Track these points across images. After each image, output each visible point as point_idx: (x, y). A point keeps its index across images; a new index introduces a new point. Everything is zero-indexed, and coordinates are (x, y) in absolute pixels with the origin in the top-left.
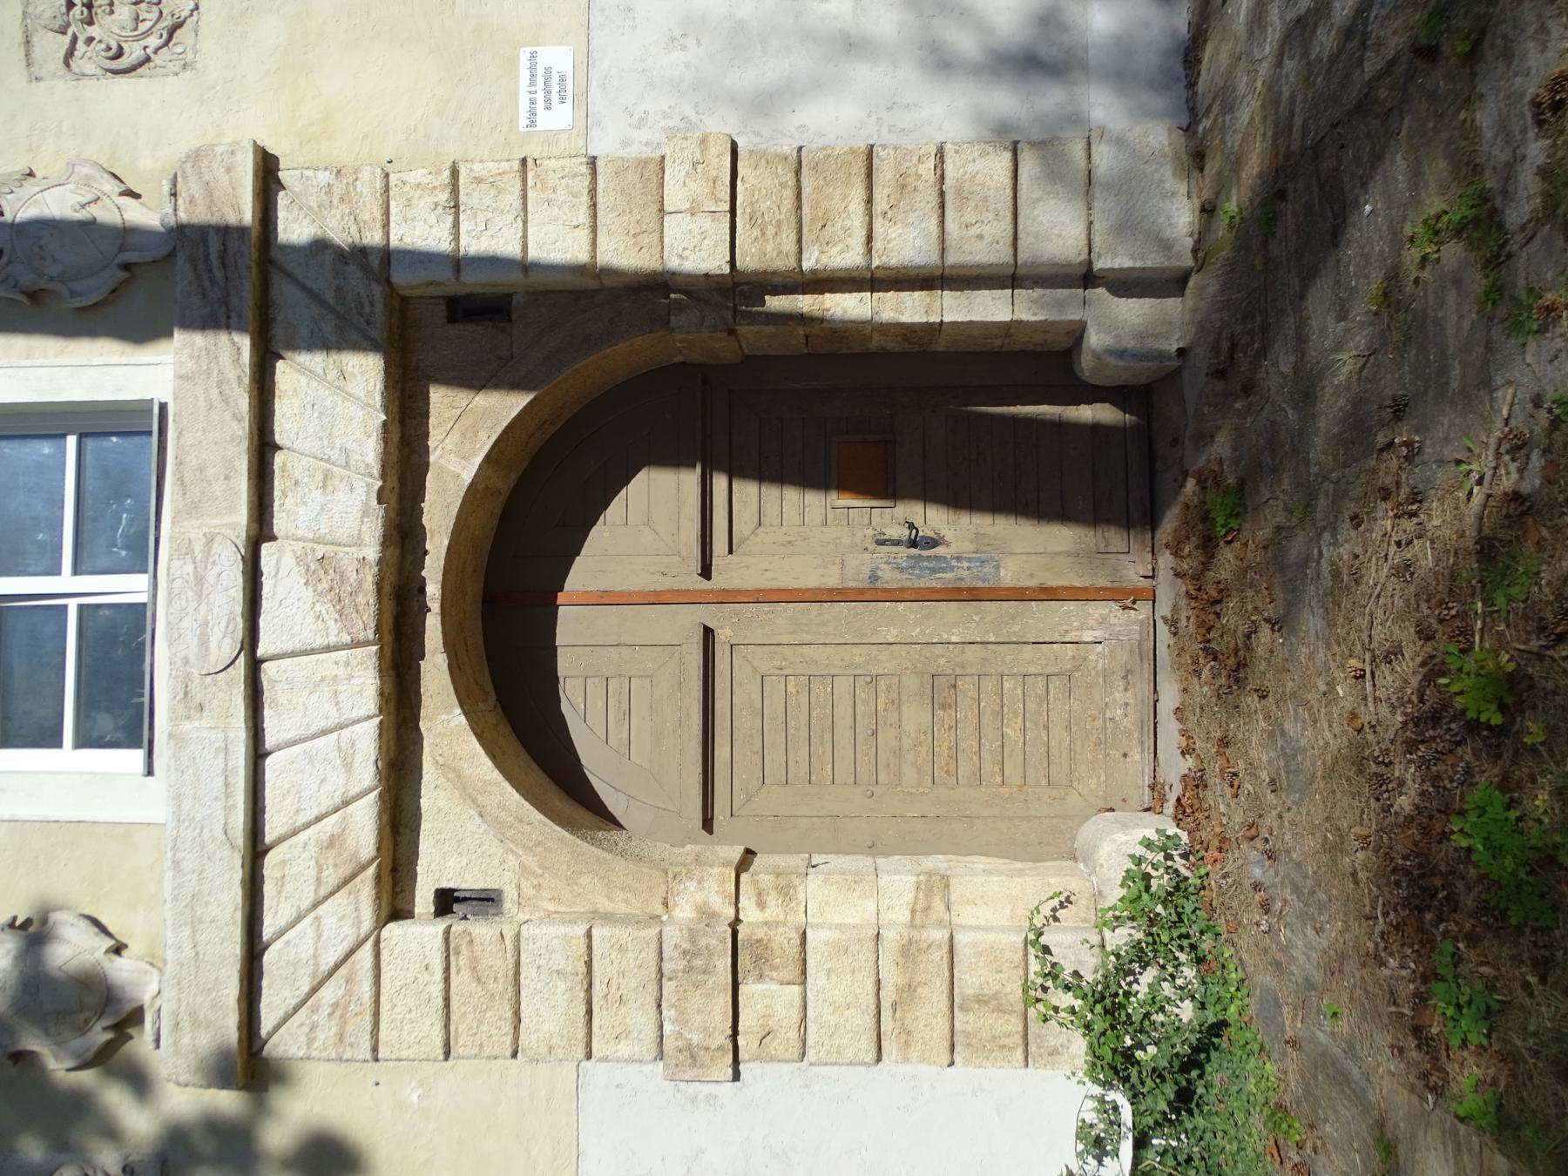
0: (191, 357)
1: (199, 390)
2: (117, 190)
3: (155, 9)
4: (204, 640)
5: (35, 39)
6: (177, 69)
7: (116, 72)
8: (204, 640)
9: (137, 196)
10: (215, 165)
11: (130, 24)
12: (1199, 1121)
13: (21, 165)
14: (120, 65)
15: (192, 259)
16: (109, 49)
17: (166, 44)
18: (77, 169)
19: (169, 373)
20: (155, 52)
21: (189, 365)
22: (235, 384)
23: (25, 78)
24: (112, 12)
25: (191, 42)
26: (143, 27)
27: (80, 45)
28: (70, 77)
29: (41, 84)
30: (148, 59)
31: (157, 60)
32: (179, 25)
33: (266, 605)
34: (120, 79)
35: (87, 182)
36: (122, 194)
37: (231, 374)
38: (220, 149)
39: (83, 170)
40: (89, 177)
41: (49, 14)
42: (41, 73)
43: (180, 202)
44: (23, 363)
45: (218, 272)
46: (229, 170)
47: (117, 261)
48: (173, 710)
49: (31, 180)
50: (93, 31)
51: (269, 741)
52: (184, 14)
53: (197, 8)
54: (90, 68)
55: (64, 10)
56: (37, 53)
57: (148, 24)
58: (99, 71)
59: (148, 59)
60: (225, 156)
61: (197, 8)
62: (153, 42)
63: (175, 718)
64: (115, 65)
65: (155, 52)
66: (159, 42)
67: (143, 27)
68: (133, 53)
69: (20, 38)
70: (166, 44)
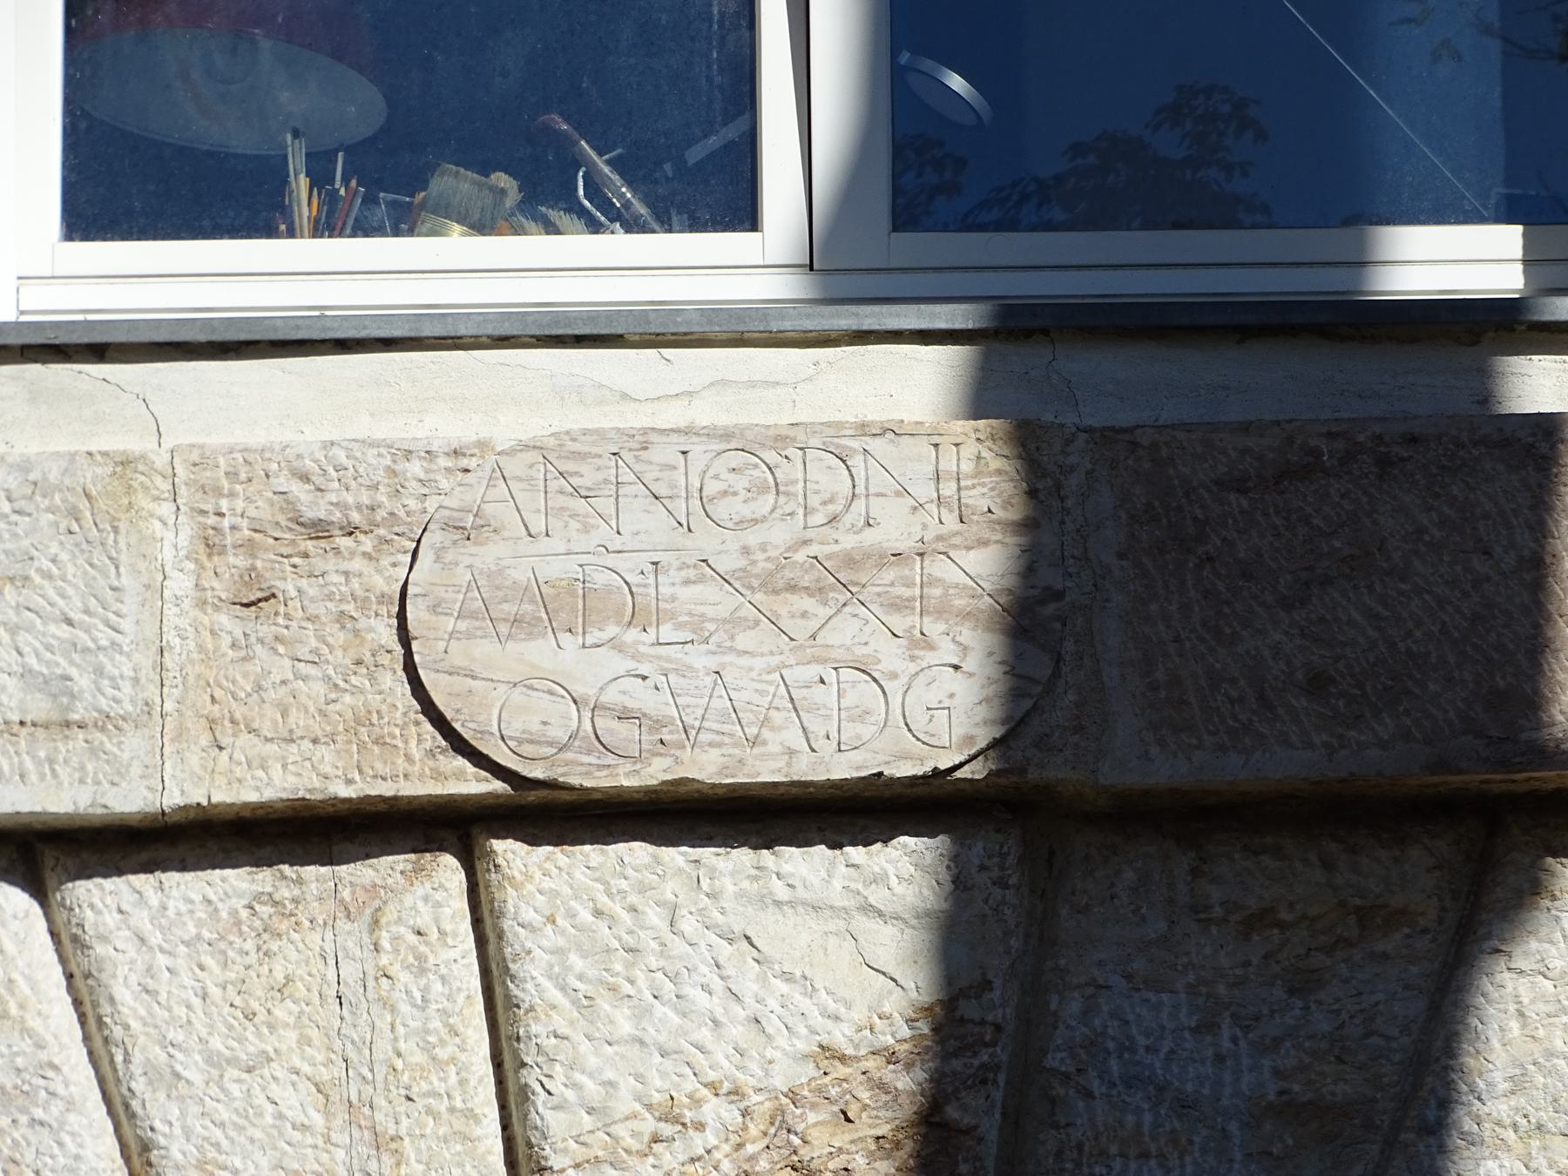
4: (562, 608)
8: (562, 608)
33: (730, 865)
48: (248, 467)
51: (101, 900)
63: (207, 480)
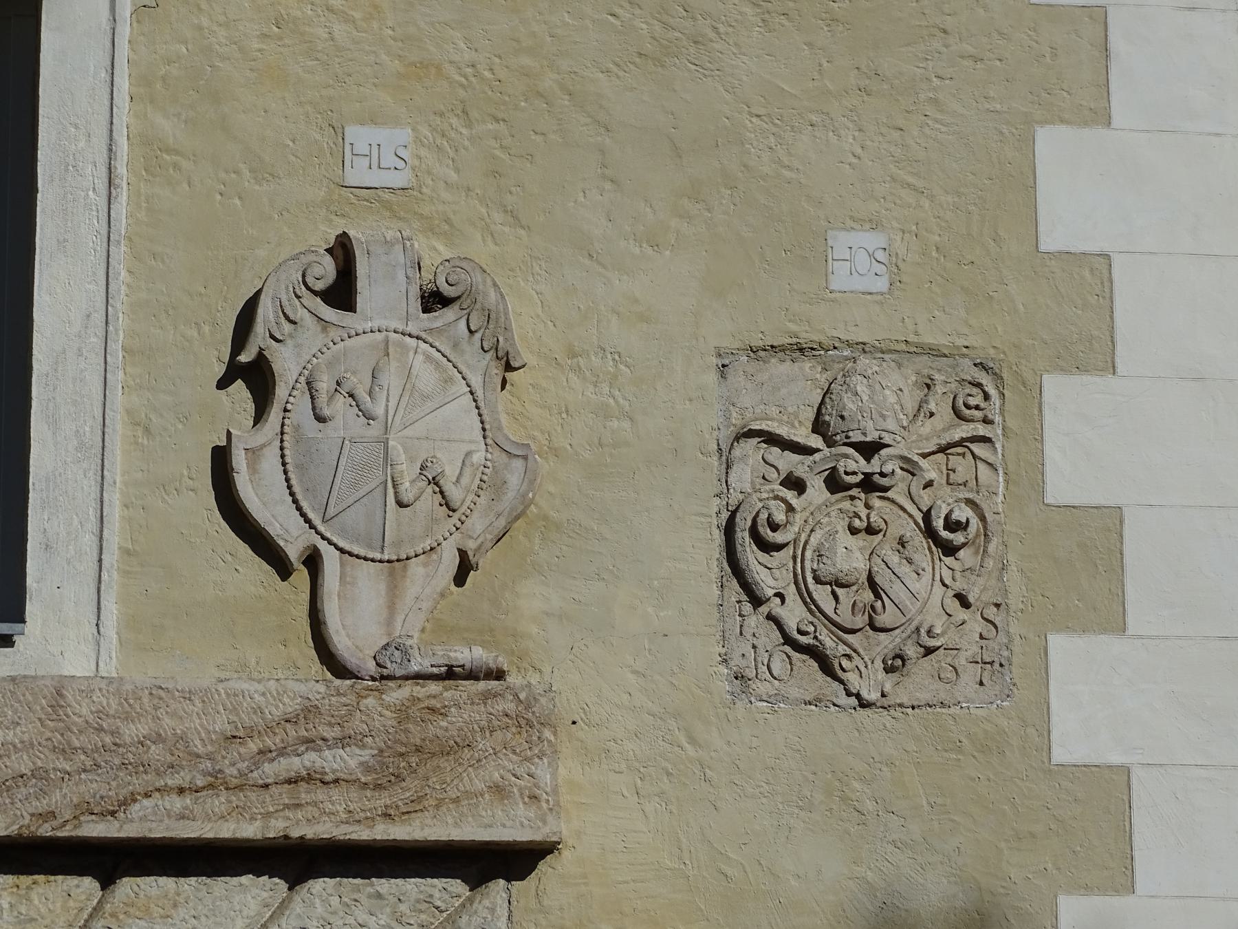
0: (101, 713)
1: (28, 730)
2: (470, 546)
3: (860, 621)
5: (807, 365)
6: (736, 661)
7: (729, 530)
9: (460, 578)
10: (509, 762)
11: (826, 570)
12: (908, 535)
13: (524, 354)
14: (742, 540)
15: (310, 711)
16: (774, 527)
17: (788, 640)
18: (518, 464)
19: (77, 665)
20: (770, 617)
21: (83, 709)
22: (41, 805)
23: (728, 343)
24: (853, 531)
25: (794, 692)
26: (822, 595)
27: (788, 461)
28: (726, 434)
29: (712, 377)
30: (757, 601)
31: (755, 620)
32: (826, 666)
34: (718, 537)
35: (491, 484)
36: (463, 554)
37: (60, 798)
38: (543, 772)
39: (514, 476)
40: (499, 487)
41: (850, 405)
42: (736, 378)
43: (433, 687)
44: (116, 347)
45: (270, 770)
46: (499, 791)
47: (323, 546)
49: (496, 372)
50: (817, 490)
52: (852, 678)
53: (864, 704)
54: (743, 477)
55: (856, 437)
56: (780, 368)
57: (828, 606)
58: (735, 497)
59: (757, 601)
60: (525, 782)
61: (864, 704)
62: (794, 614)
64: (743, 536)
65: (770, 617)
66: (791, 625)
67: (822, 595)
68: (768, 574)
69: (807, 336)
70: (788, 640)
